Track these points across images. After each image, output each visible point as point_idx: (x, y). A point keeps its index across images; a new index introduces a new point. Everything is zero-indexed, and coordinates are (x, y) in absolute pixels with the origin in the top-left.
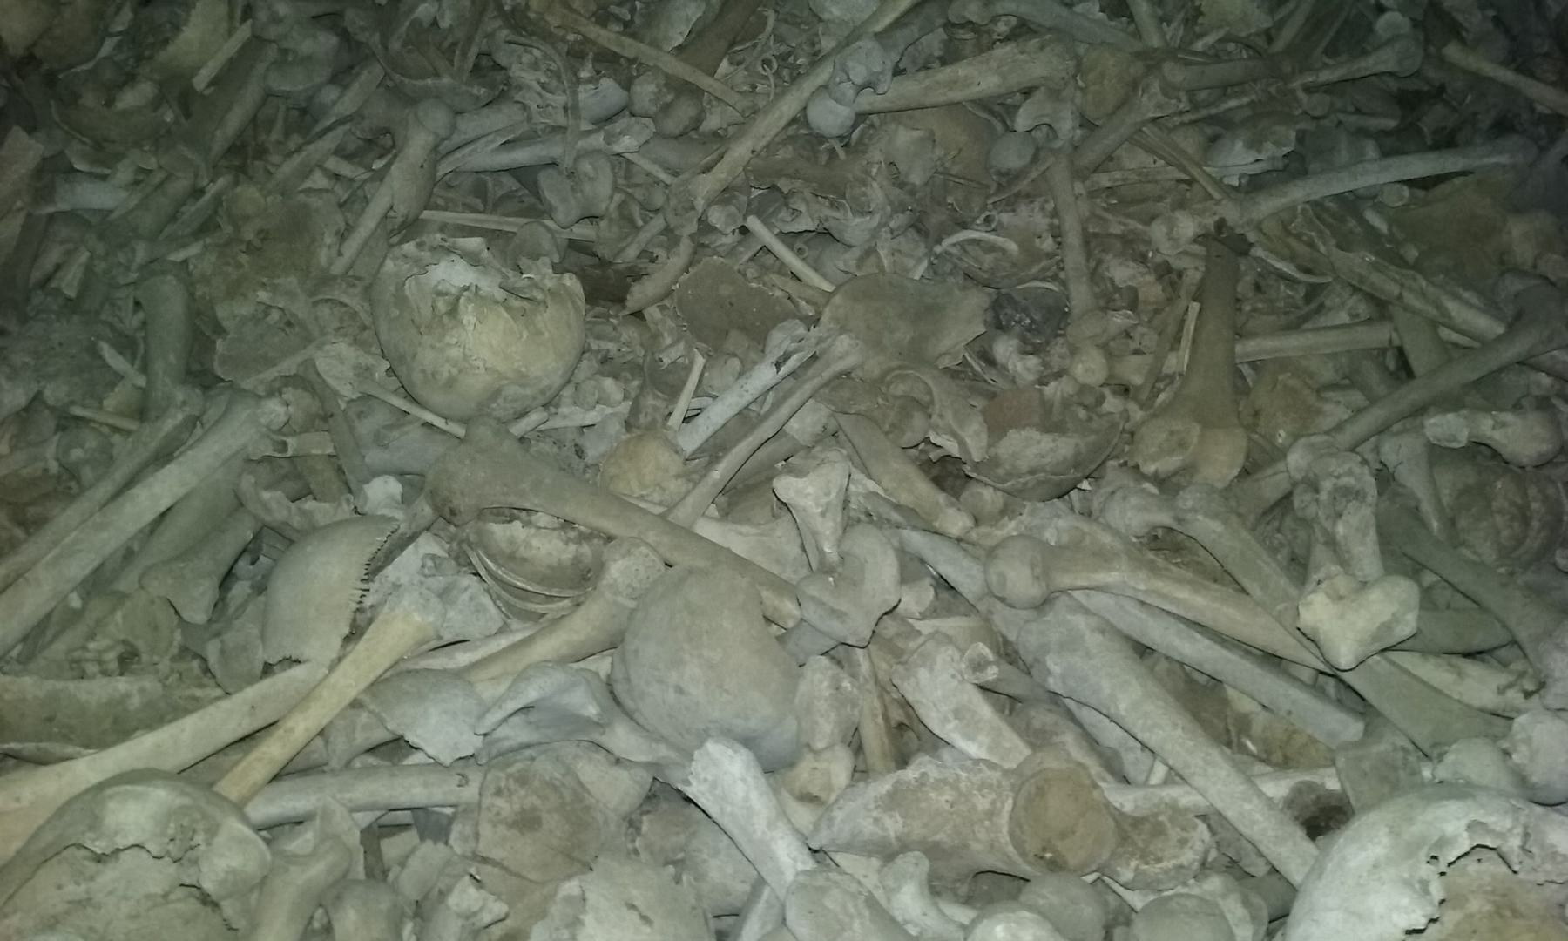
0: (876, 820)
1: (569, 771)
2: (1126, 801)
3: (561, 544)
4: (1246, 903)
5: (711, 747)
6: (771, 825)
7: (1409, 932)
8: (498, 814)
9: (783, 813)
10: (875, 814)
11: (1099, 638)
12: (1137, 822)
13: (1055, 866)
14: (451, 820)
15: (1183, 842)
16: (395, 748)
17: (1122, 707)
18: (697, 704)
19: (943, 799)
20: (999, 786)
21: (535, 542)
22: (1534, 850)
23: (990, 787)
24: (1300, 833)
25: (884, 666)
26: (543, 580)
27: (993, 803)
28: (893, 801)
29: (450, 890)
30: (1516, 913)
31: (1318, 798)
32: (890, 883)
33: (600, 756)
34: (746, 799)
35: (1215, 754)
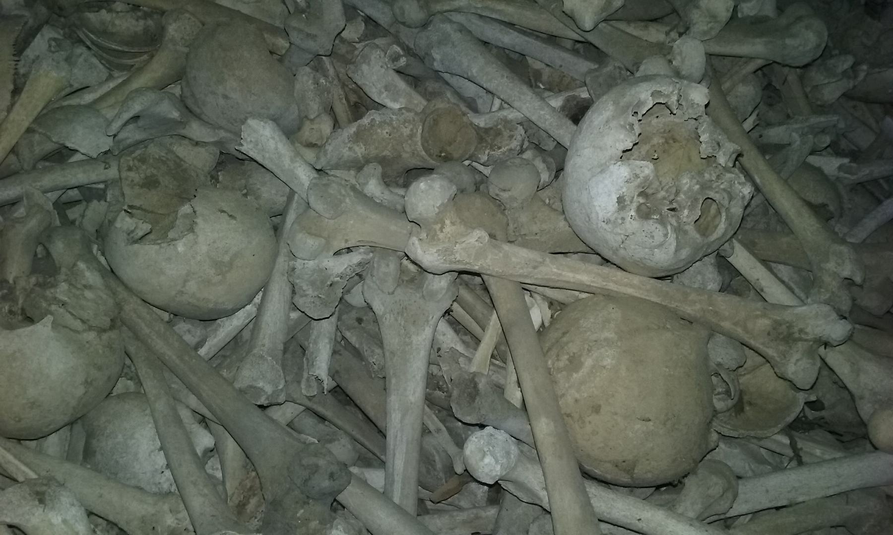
0: (350, 149)
1: (170, 151)
2: (481, 121)
3: (134, 22)
4: (544, 161)
5: (251, 122)
6: (292, 161)
7: (624, 152)
8: (132, 181)
9: (298, 154)
10: (349, 145)
11: (459, 35)
12: (487, 130)
13: (447, 159)
14: (104, 191)
15: (511, 137)
16: (61, 155)
17: (474, 71)
18: (238, 103)
19: (384, 132)
20: (414, 120)
21: (117, 22)
22: (683, 103)
23: (409, 121)
24: (569, 122)
25: (343, 70)
26: (127, 44)
27: (412, 130)
28: (358, 137)
29: (115, 219)
30: (675, 140)
31: (578, 102)
32: (361, 181)
33: (186, 142)
34: (276, 149)
35: (525, 88)
